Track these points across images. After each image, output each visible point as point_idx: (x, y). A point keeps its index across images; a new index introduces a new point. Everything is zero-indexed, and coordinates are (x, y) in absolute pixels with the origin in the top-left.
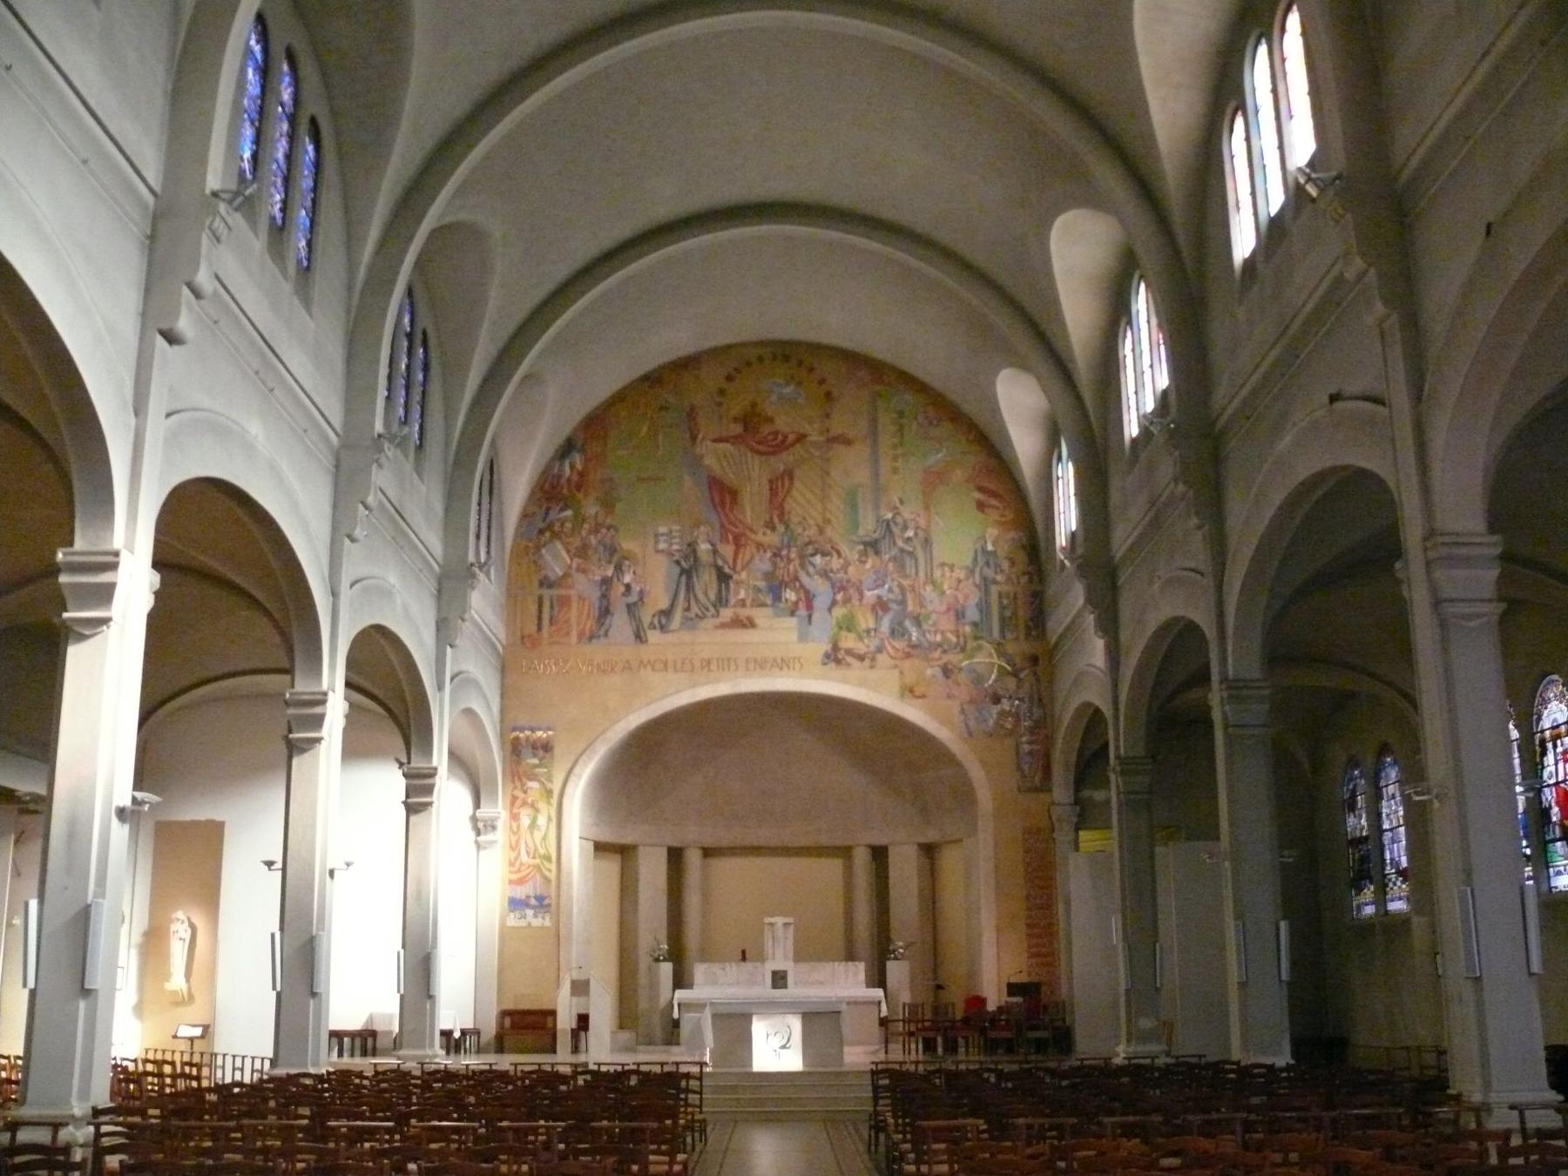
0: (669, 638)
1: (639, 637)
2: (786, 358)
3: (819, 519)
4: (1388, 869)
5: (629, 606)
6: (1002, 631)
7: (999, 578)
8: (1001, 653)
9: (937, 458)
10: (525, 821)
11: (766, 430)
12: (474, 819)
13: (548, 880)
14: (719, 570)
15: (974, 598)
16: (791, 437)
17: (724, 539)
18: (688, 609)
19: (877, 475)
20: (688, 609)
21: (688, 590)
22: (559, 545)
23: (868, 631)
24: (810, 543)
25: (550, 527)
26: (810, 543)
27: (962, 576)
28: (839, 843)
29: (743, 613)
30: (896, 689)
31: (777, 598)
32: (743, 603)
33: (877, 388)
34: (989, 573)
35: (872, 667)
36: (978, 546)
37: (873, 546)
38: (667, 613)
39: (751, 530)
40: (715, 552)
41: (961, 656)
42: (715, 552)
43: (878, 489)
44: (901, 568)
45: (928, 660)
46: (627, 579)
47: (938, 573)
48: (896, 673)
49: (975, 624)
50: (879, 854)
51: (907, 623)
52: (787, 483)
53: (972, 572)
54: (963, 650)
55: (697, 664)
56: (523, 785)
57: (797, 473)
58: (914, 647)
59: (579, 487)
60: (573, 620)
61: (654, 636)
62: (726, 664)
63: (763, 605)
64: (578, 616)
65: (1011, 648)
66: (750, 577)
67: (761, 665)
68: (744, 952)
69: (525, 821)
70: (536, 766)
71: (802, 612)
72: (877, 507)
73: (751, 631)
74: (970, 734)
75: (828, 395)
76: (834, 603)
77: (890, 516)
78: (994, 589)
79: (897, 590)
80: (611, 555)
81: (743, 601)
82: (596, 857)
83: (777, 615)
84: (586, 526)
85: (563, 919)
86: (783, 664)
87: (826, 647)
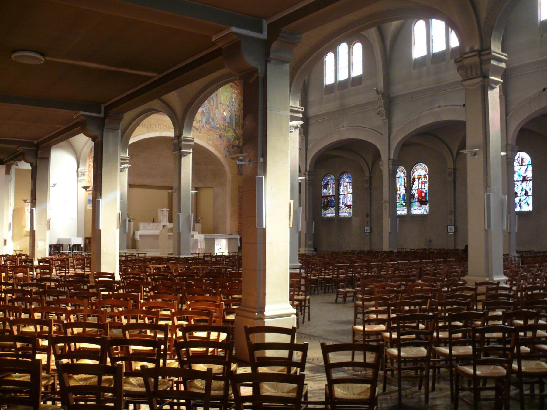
4: (341, 205)
6: (235, 126)
8: (235, 133)
12: (78, 172)
23: (199, 121)
28: (170, 186)
41: (224, 132)
49: (228, 123)
51: (210, 120)
54: (225, 130)
65: (237, 131)
68: (154, 219)
74: (226, 156)
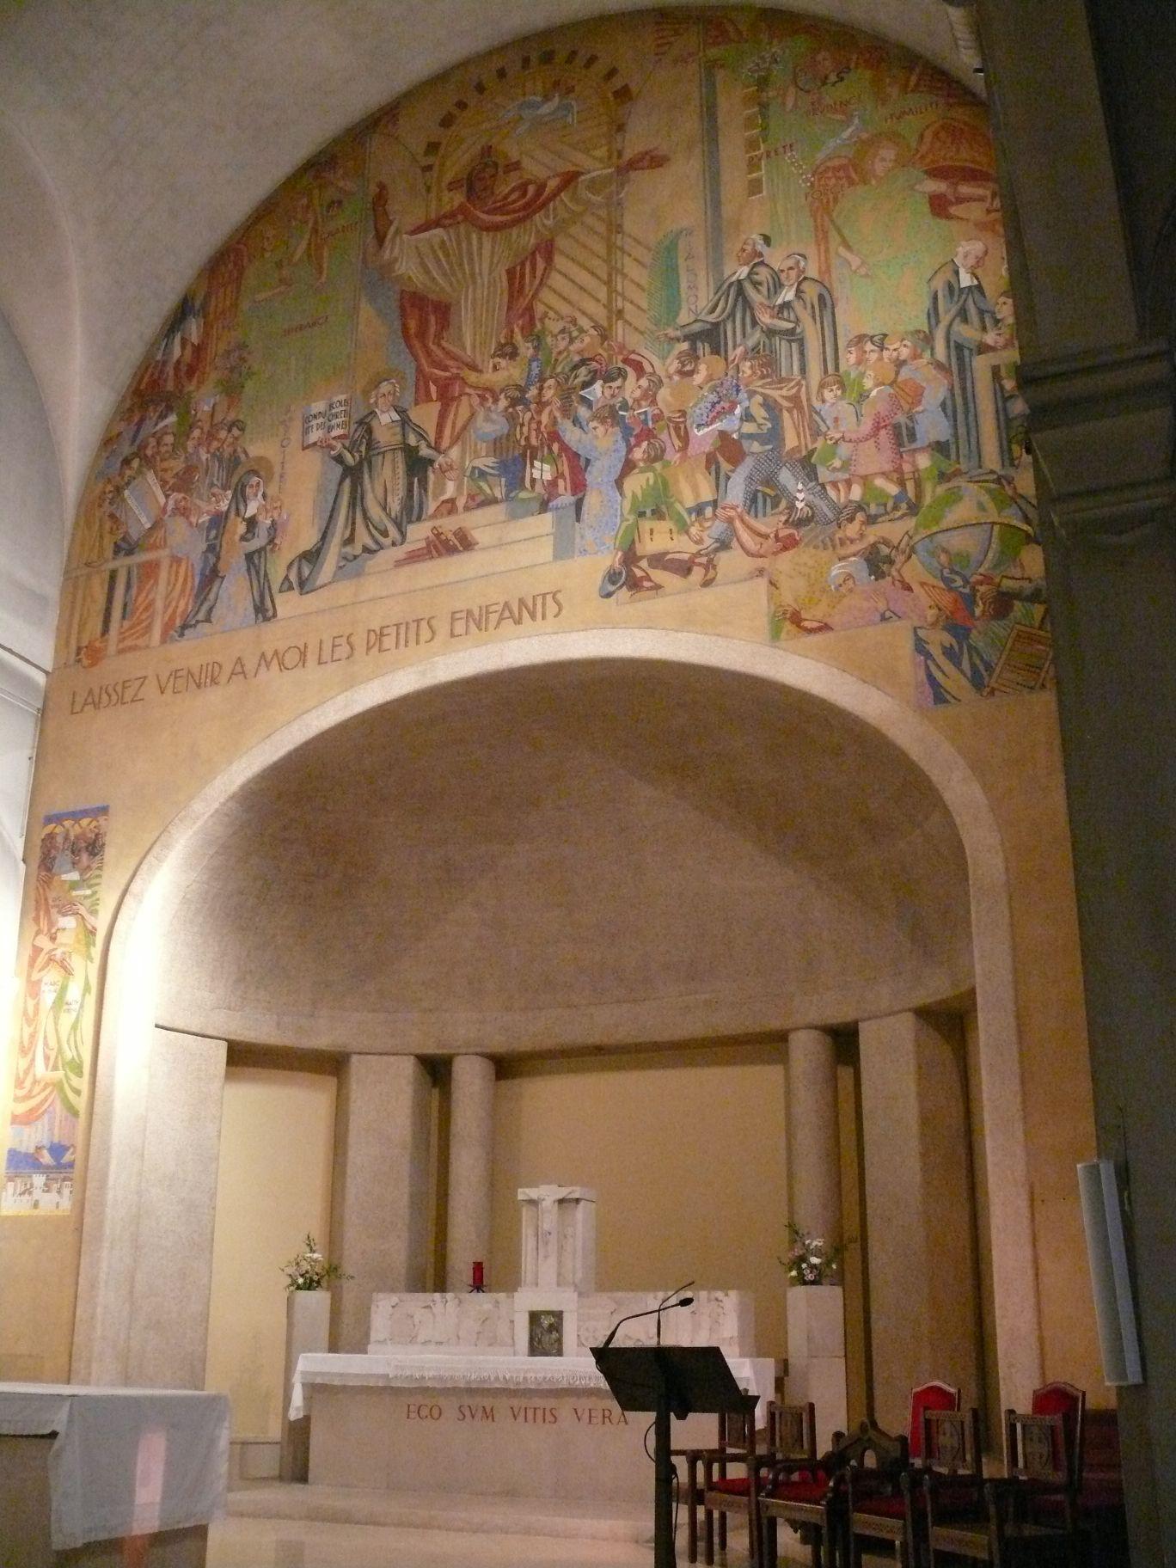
0: (312, 601)
1: (263, 611)
2: (548, 58)
3: (600, 314)
5: (249, 557)
7: (990, 338)
9: (838, 141)
10: (48, 997)
11: (505, 187)
13: (75, 1113)
14: (411, 454)
15: (936, 391)
16: (553, 184)
17: (422, 397)
18: (350, 541)
19: (715, 203)
20: (350, 541)
21: (352, 505)
22: (151, 477)
23: (699, 510)
24: (583, 362)
25: (140, 453)
26: (583, 362)
27: (905, 353)
29: (448, 525)
30: (763, 622)
31: (516, 481)
32: (450, 507)
33: (713, 52)
34: (968, 333)
35: (707, 583)
36: (939, 284)
37: (711, 337)
38: (312, 556)
39: (473, 368)
40: (405, 422)
42: (405, 422)
43: (717, 231)
44: (767, 363)
45: (832, 544)
46: (252, 509)
47: (849, 359)
48: (762, 584)
50: (843, 1042)
51: (785, 477)
52: (541, 265)
53: (929, 339)
55: (359, 641)
56: (51, 924)
57: (561, 242)
58: (800, 523)
59: (191, 371)
60: (159, 604)
61: (287, 605)
62: (413, 631)
63: (491, 501)
64: (167, 594)
66: (465, 459)
67: (478, 620)
69: (48, 997)
70: (74, 886)
71: (566, 498)
72: (716, 264)
73: (465, 556)
75: (624, 94)
76: (629, 466)
77: (743, 272)
78: (981, 366)
79: (760, 413)
80: (230, 474)
81: (452, 501)
82: (229, 1077)
83: (513, 516)
84: (196, 433)
85: (92, 1186)
86: (521, 611)
87: (609, 559)
